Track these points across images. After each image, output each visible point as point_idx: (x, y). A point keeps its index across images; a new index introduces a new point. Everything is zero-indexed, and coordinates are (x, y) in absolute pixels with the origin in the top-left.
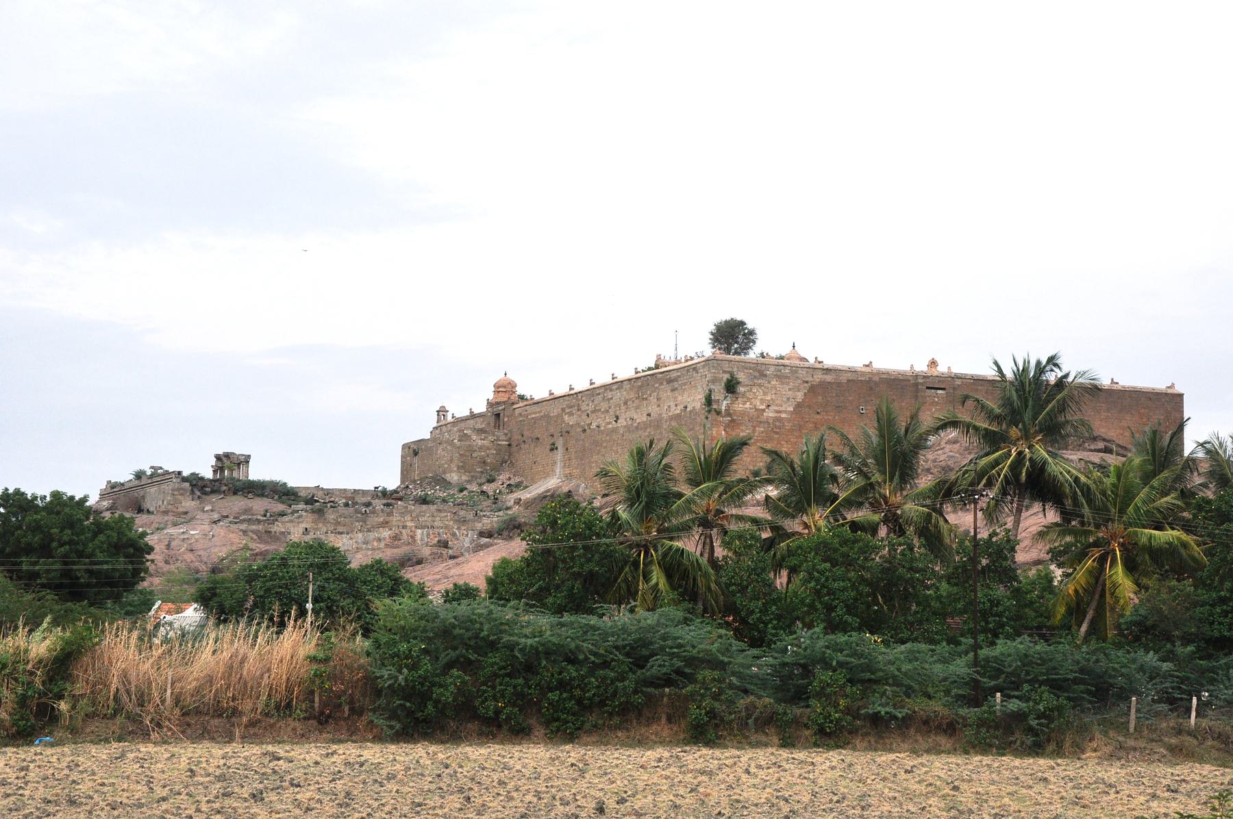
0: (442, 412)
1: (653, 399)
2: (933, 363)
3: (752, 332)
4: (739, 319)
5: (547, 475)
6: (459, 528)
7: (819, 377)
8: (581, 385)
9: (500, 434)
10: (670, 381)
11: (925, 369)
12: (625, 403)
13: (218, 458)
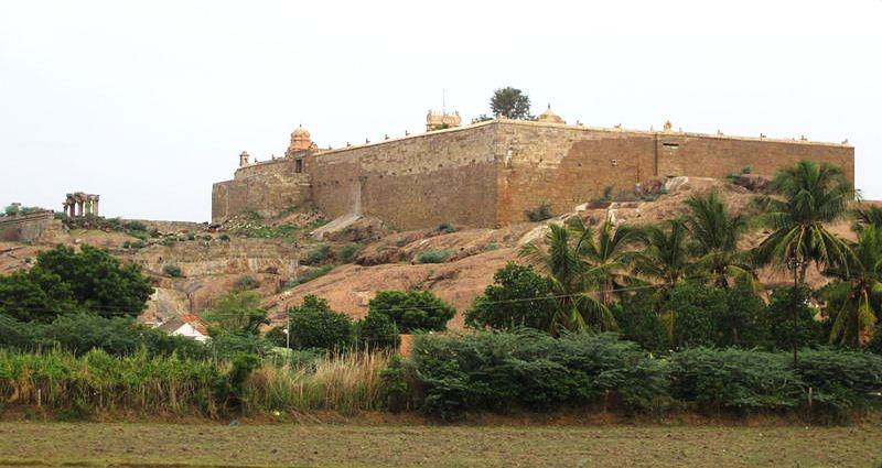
0: (243, 157)
1: (444, 153)
2: (668, 125)
3: (526, 99)
4: (516, 88)
5: (346, 209)
6: (282, 258)
7: (580, 136)
8: (377, 139)
9: (302, 176)
10: (459, 139)
11: (662, 129)
12: (419, 156)
13: (69, 197)
